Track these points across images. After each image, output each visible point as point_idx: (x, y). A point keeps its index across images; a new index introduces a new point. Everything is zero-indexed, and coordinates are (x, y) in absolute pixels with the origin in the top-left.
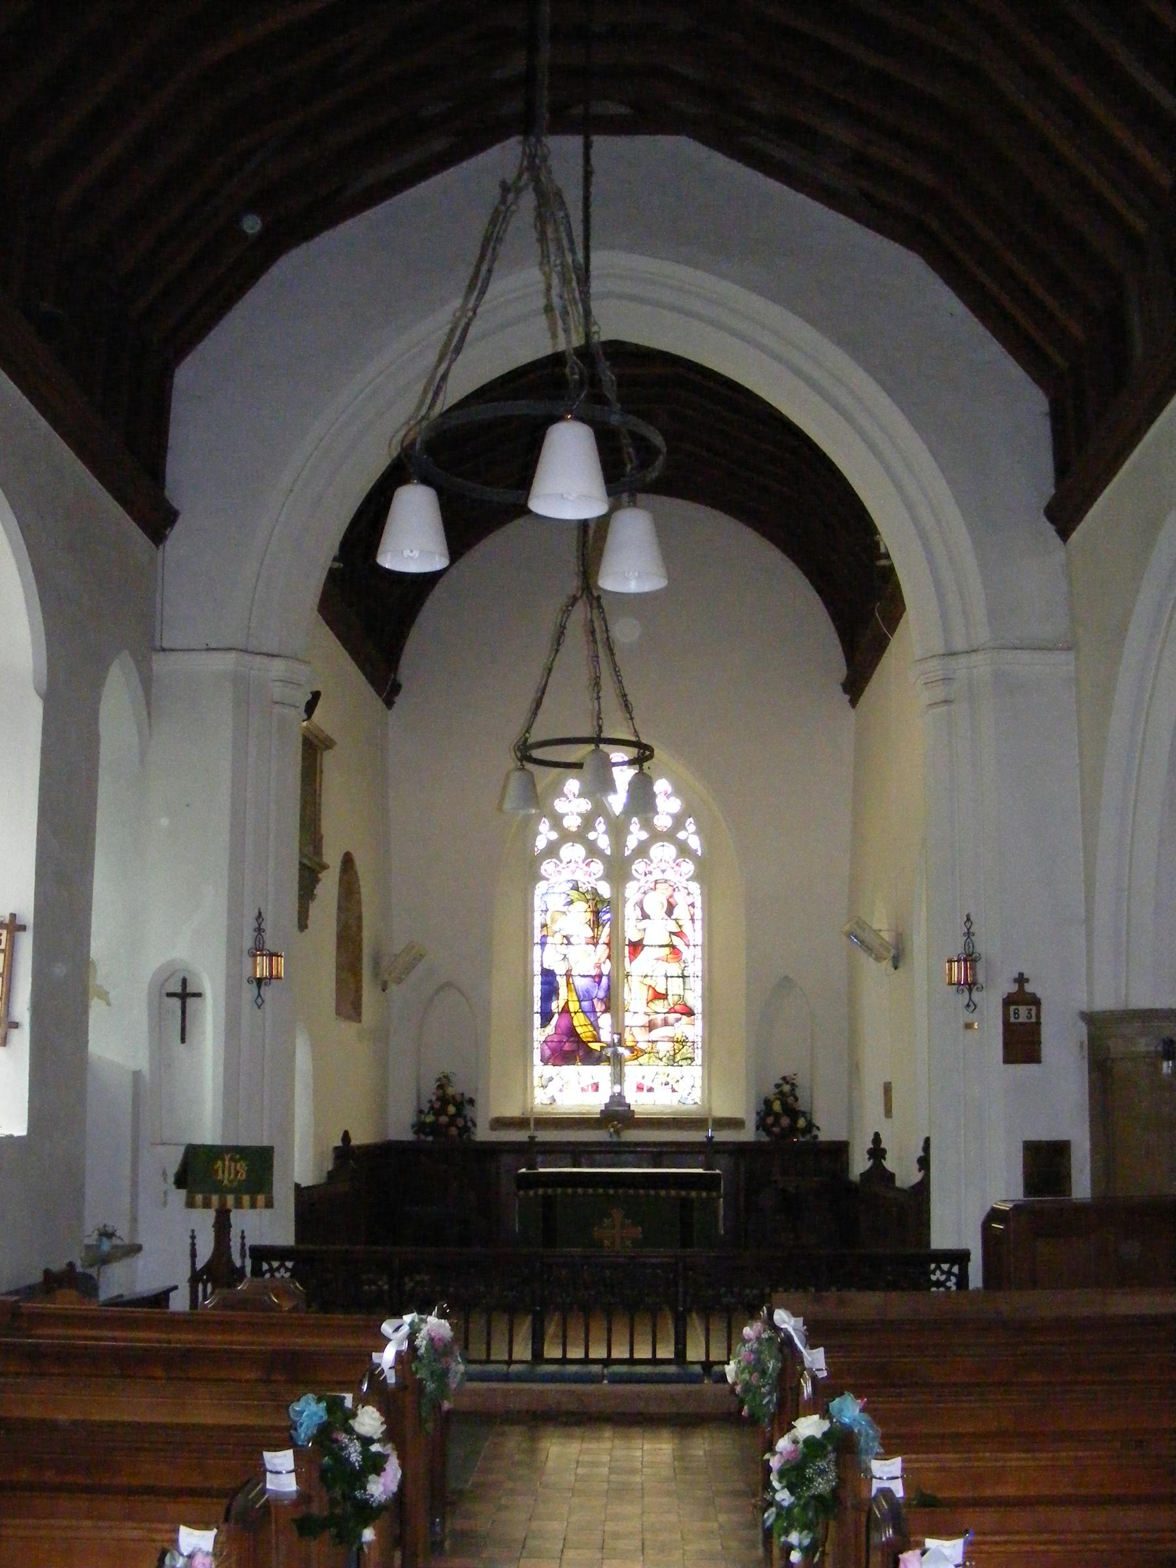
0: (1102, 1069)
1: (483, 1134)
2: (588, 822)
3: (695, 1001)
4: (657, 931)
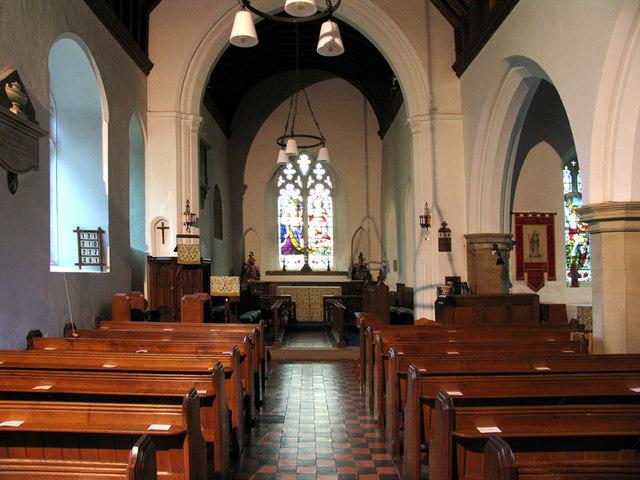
0: (472, 254)
1: (264, 278)
2: (295, 176)
3: (331, 235)
4: (318, 212)
